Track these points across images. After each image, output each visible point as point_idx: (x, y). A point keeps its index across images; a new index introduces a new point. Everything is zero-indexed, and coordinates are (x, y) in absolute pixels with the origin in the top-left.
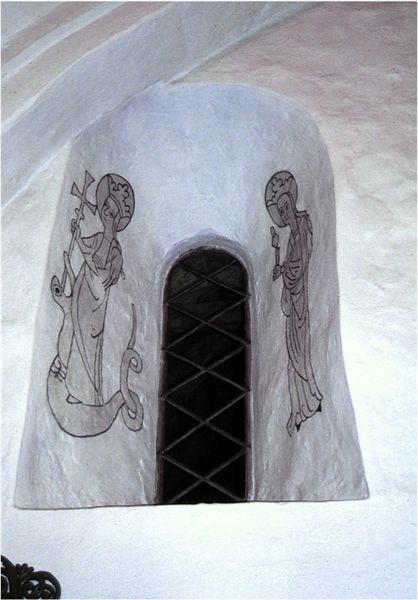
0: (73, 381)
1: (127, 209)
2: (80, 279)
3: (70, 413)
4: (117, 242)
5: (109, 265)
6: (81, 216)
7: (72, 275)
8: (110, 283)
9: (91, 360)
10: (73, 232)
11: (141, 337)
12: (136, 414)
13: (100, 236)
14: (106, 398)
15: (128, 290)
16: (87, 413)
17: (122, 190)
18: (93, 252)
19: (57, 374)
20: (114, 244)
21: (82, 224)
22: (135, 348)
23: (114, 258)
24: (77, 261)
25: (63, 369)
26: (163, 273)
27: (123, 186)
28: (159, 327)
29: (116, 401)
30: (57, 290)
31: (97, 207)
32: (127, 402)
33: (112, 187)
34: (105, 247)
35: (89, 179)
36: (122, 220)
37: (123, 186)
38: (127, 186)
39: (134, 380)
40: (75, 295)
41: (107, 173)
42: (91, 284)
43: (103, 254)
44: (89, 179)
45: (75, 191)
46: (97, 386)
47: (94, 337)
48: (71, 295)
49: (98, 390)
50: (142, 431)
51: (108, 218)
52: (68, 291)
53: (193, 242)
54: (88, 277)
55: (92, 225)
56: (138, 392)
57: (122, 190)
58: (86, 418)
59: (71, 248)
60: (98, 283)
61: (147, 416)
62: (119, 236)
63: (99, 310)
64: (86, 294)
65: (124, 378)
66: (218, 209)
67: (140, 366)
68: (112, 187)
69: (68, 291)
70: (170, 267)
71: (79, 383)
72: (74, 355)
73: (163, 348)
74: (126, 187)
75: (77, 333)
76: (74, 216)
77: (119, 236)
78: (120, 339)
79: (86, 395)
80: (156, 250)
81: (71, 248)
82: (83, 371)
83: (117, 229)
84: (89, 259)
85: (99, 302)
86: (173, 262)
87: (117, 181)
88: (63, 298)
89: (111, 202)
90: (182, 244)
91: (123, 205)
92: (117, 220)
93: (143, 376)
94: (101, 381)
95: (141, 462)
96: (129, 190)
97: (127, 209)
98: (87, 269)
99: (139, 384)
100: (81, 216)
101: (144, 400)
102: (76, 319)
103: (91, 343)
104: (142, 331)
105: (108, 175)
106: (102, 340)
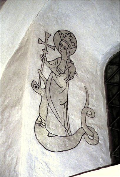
0: (50, 126)
1: (73, 44)
2: (49, 80)
3: (50, 142)
4: (71, 60)
5: (67, 71)
6: (45, 52)
7: (44, 79)
8: (68, 79)
9: (61, 115)
10: (42, 60)
11: (92, 101)
12: (95, 141)
13: (59, 60)
14: (73, 132)
15: (82, 80)
16: (61, 140)
17: (68, 36)
18: (56, 66)
19: (40, 125)
20: (69, 61)
21: (47, 55)
22: (90, 106)
23: (69, 68)
24: (46, 73)
25: (43, 121)
26: (101, 69)
27: (68, 34)
28: (103, 94)
29: (80, 132)
30: (36, 87)
31: (55, 46)
32: (87, 133)
33: (62, 36)
34: (63, 64)
35: (47, 35)
36: (71, 50)
37: (68, 34)
38: (70, 34)
39: (90, 121)
40: (48, 88)
41: (58, 30)
42: (57, 81)
43: (62, 67)
44: (47, 35)
45: (40, 41)
46: (66, 127)
47: (62, 105)
48: (45, 88)
49: (67, 129)
50: (98, 144)
51: (63, 50)
52: (43, 86)
53: (113, 51)
54: (54, 78)
55: (53, 55)
56: (93, 126)
57: (68, 36)
58: (61, 143)
59: (42, 67)
60: (61, 81)
61: (101, 137)
62: (71, 57)
63: (65, 92)
64: (54, 86)
65: (84, 121)
66: (100, 36)
67: (93, 114)
68: (62, 36)
69: (43, 86)
70: (105, 66)
71: (54, 126)
72: (49, 114)
73: (107, 104)
74: (70, 35)
75: (51, 105)
76: (42, 53)
77: (71, 57)
78: (79, 103)
79: (61, 132)
80: (94, 59)
81: (42, 67)
82: (56, 121)
83: (69, 55)
84: (54, 70)
85: (63, 89)
86: (106, 63)
87: (64, 33)
88: (40, 90)
89: (63, 43)
90: (107, 53)
91: (70, 43)
92: (68, 50)
93: (96, 119)
94: (68, 124)
95: (100, 159)
96: (72, 35)
97: (73, 44)
98: (54, 75)
99: (94, 123)
100: (45, 52)
101: (97, 130)
102: (49, 98)
103: (60, 110)
104: (92, 98)
105: (59, 31)
106: (67, 106)
